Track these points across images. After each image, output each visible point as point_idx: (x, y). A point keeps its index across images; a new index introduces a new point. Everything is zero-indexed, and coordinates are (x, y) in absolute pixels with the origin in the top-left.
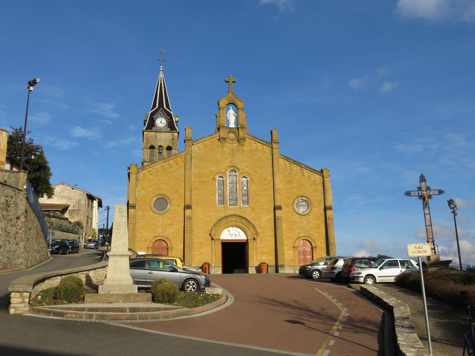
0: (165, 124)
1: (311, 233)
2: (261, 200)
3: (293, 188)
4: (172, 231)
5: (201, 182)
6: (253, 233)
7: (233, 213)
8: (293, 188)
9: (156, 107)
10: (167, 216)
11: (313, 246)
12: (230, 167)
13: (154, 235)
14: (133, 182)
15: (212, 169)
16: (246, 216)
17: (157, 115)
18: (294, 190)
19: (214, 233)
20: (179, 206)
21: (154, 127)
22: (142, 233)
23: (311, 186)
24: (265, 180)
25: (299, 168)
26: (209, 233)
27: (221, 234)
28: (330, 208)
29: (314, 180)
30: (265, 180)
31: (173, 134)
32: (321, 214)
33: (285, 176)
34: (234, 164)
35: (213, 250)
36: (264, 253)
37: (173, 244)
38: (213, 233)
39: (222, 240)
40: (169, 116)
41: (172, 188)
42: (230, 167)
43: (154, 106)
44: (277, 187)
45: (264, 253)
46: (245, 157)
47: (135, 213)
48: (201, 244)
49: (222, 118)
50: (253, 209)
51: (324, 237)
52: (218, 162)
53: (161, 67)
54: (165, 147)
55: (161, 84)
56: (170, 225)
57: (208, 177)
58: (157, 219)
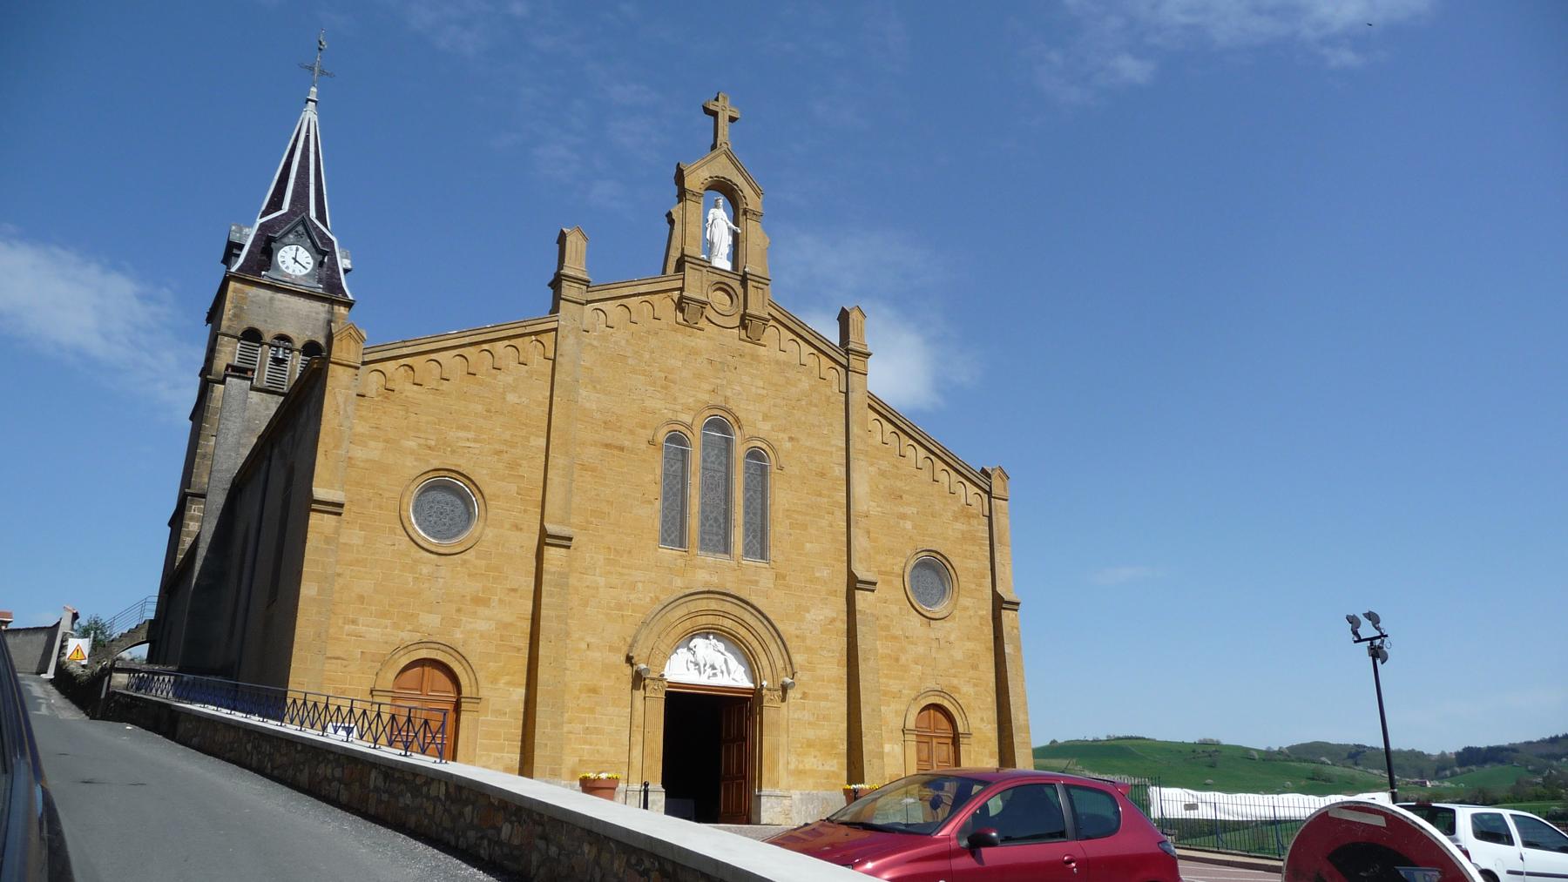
0: (310, 267)
1: (955, 681)
3: (903, 517)
4: (482, 626)
5: (607, 446)
7: (715, 582)
8: (903, 517)
10: (465, 562)
11: (961, 730)
13: (407, 636)
14: (341, 399)
15: (647, 403)
16: (753, 600)
18: (909, 525)
19: (645, 652)
20: (517, 528)
22: (354, 622)
23: (956, 519)
24: (823, 475)
25: (922, 452)
26: (625, 650)
27: (667, 657)
29: (963, 501)
30: (823, 475)
31: (331, 312)
33: (883, 474)
37: (482, 683)
38: (640, 654)
39: (671, 684)
43: (275, 203)
44: (859, 506)
45: (810, 744)
47: (337, 531)
48: (594, 690)
50: (779, 577)
51: (990, 699)
53: (314, 89)
54: (299, 345)
55: (307, 137)
57: (631, 432)
58: (425, 571)
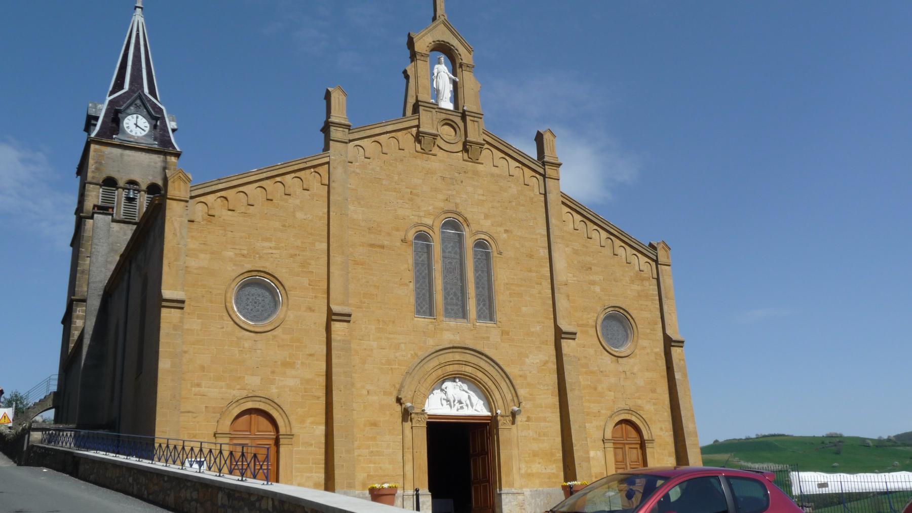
0: (147, 129)
2: (524, 309)
3: (593, 283)
4: (291, 382)
5: (372, 245)
6: (509, 397)
8: (593, 283)
9: (122, 88)
10: (275, 337)
11: (646, 437)
17: (128, 107)
18: (597, 289)
20: (311, 309)
21: (117, 134)
22: (198, 385)
23: (632, 282)
25: (604, 234)
26: (395, 394)
27: (426, 397)
28: (680, 343)
29: (637, 268)
31: (165, 162)
32: (656, 354)
33: (576, 252)
34: (457, 205)
35: (406, 446)
36: (535, 454)
38: (406, 396)
39: (431, 416)
40: (155, 118)
43: (119, 85)
44: (560, 277)
45: (535, 454)
47: (181, 320)
48: (375, 424)
50: (504, 333)
52: (417, 195)
54: (144, 187)
55: (138, 35)
56: (285, 364)
57: (389, 234)
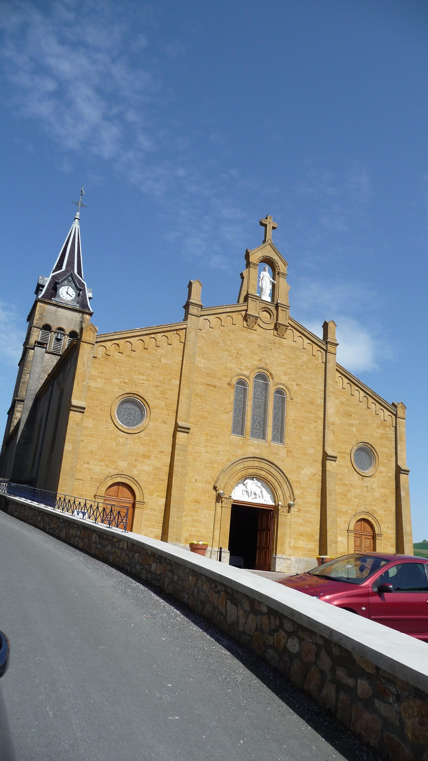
0: (74, 296)
2: (304, 437)
3: (352, 425)
4: (146, 468)
5: (208, 385)
8: (352, 425)
10: (140, 437)
12: (259, 368)
13: (113, 471)
18: (354, 429)
20: (164, 422)
22: (88, 463)
23: (378, 427)
26: (213, 483)
28: (407, 472)
29: (382, 418)
31: (83, 318)
33: (342, 403)
35: (217, 518)
36: (301, 534)
37: (146, 495)
40: (80, 289)
41: (157, 386)
42: (259, 368)
43: (59, 266)
45: (301, 534)
46: (283, 357)
47: (82, 420)
48: (198, 502)
49: (253, 281)
52: (241, 355)
53: (78, 213)
54: (67, 332)
55: (74, 236)
56: (145, 456)
57: (220, 379)
